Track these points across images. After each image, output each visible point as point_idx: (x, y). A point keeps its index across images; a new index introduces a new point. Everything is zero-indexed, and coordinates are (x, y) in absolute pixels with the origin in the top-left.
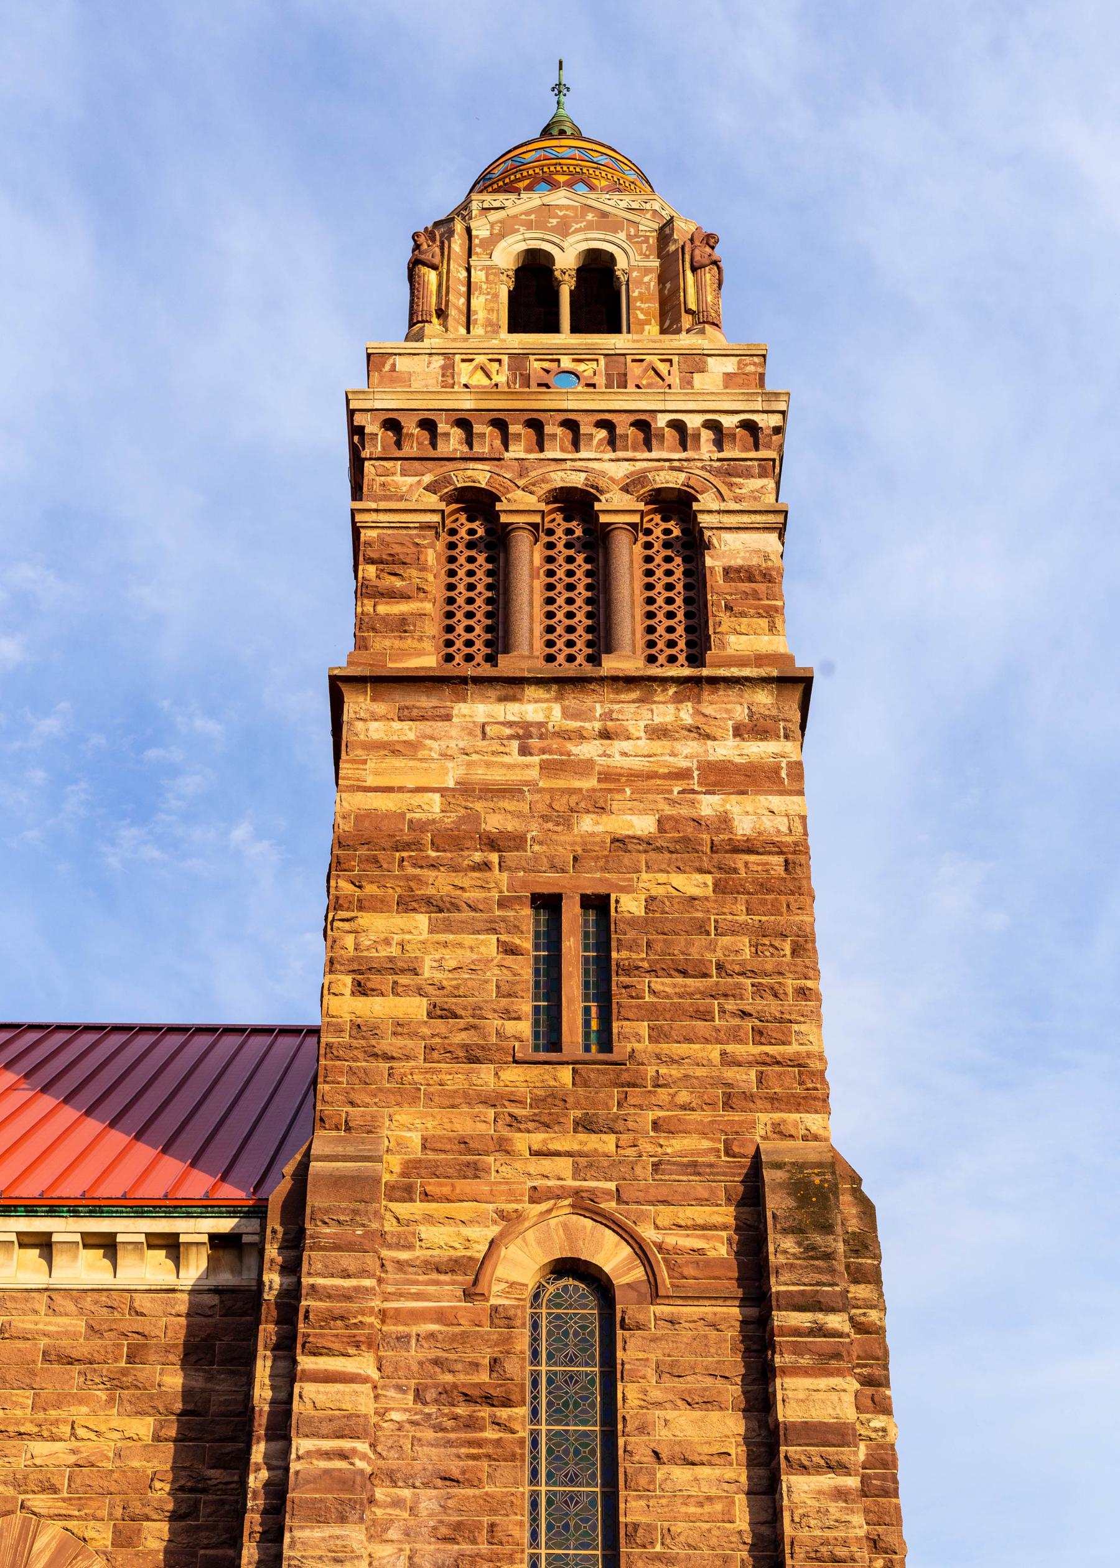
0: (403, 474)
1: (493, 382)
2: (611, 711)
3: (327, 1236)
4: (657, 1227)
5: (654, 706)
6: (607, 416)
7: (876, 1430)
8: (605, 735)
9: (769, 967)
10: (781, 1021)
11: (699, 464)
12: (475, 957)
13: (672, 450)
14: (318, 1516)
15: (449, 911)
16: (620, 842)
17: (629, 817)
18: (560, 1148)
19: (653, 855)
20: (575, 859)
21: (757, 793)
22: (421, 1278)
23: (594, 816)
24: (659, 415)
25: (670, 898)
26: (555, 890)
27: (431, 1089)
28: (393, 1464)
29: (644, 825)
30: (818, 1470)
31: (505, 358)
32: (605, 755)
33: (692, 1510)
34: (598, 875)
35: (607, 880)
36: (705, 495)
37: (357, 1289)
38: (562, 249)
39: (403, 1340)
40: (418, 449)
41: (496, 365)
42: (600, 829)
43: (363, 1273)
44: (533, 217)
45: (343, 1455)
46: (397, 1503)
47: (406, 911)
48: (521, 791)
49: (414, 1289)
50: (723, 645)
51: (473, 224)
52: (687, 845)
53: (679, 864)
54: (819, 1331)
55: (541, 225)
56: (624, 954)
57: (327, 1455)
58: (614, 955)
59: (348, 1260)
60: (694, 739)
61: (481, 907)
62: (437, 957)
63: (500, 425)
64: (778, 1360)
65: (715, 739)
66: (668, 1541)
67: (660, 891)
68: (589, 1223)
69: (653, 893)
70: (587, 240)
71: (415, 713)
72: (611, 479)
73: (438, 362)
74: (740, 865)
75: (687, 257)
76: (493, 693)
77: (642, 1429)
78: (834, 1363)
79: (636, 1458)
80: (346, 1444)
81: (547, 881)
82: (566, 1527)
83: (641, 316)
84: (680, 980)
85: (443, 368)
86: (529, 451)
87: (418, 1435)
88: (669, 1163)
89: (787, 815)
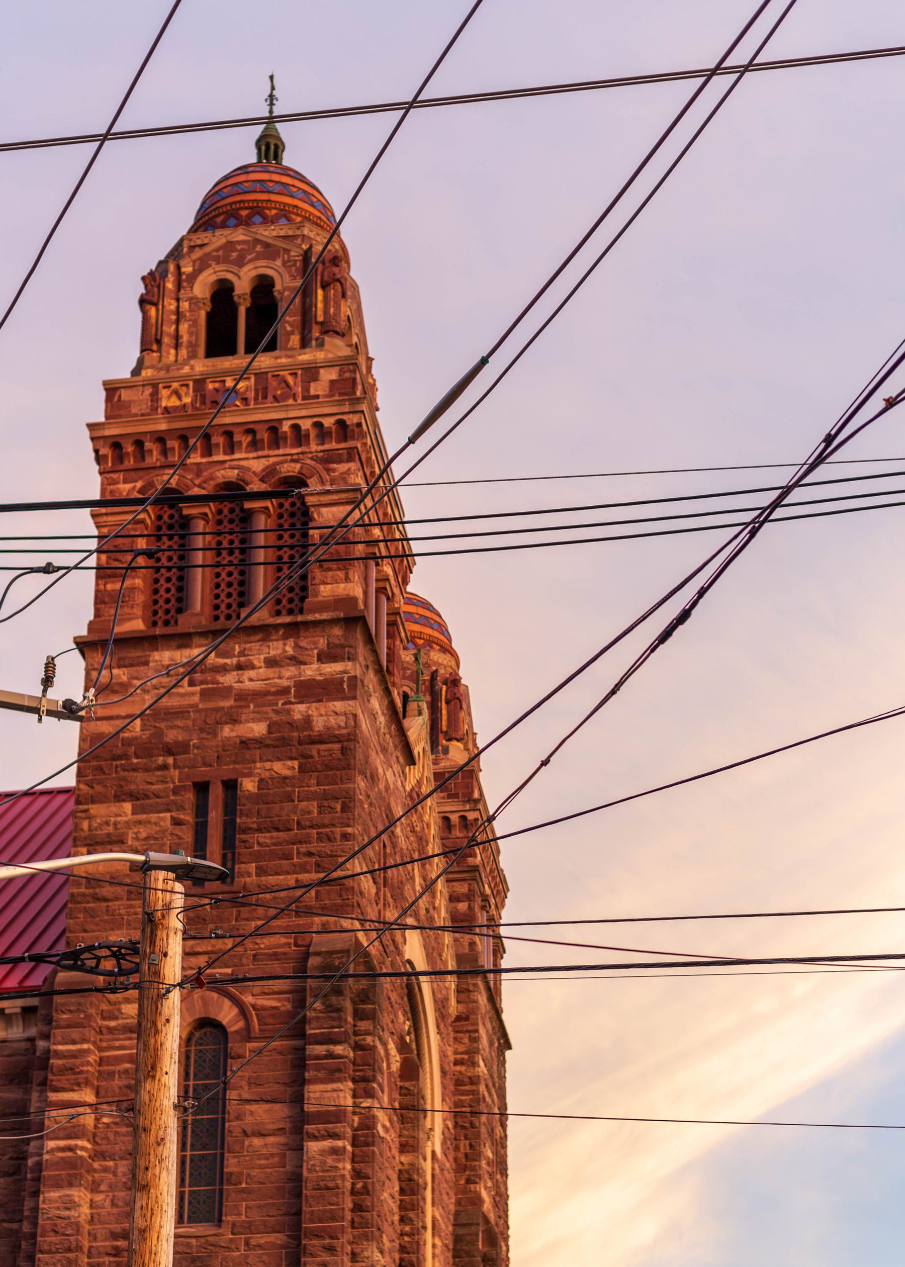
0: (125, 482)
1: (183, 403)
2: (245, 649)
3: (64, 1020)
4: (253, 995)
5: (270, 644)
6: (251, 426)
7: (364, 1108)
8: (240, 667)
9: (326, 822)
10: (331, 856)
11: (310, 456)
12: (158, 829)
13: (293, 446)
14: (58, 1185)
15: (143, 799)
16: (245, 743)
17: (251, 725)
18: (200, 950)
19: (264, 750)
20: (218, 757)
21: (329, 700)
22: (122, 1036)
23: (230, 726)
24: (284, 422)
25: (272, 779)
26: (206, 779)
27: (130, 918)
28: (104, 1148)
29: (259, 729)
30: (324, 1138)
31: (191, 384)
32: (239, 681)
33: (263, 1162)
34: (231, 767)
35: (237, 769)
36: (311, 480)
37: (80, 1051)
38: (239, 277)
39: (111, 1074)
40: (135, 462)
41: (184, 388)
42: (234, 734)
43: (84, 1041)
44: (221, 253)
45: (70, 1149)
46: (106, 1170)
47: (119, 801)
48: (188, 712)
49: (117, 1044)
50: (316, 594)
51: (182, 263)
52: (284, 742)
53: (279, 755)
54: (331, 1055)
55: (226, 260)
56: (244, 819)
57: (62, 1149)
58: (238, 820)
59: (75, 1033)
60: (293, 665)
61: (161, 794)
62: (136, 830)
63: (184, 438)
64: (307, 1075)
65: (305, 664)
66: (249, 1181)
67: (266, 775)
68: (215, 995)
69: (263, 776)
70: (256, 268)
71: (127, 662)
72: (254, 473)
73: (149, 391)
74: (315, 753)
75: (319, 278)
76: (174, 644)
77: (238, 1118)
78: (337, 1075)
79: (234, 1134)
80: (72, 1142)
81: (202, 772)
82: (200, 1174)
83: (289, 328)
84: (275, 834)
85: (152, 395)
86: (202, 456)
87: (118, 1130)
88: (262, 954)
89: (345, 714)
